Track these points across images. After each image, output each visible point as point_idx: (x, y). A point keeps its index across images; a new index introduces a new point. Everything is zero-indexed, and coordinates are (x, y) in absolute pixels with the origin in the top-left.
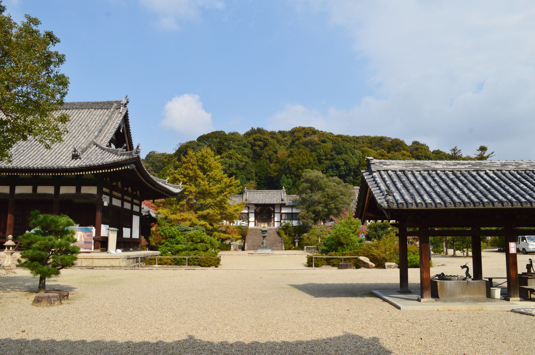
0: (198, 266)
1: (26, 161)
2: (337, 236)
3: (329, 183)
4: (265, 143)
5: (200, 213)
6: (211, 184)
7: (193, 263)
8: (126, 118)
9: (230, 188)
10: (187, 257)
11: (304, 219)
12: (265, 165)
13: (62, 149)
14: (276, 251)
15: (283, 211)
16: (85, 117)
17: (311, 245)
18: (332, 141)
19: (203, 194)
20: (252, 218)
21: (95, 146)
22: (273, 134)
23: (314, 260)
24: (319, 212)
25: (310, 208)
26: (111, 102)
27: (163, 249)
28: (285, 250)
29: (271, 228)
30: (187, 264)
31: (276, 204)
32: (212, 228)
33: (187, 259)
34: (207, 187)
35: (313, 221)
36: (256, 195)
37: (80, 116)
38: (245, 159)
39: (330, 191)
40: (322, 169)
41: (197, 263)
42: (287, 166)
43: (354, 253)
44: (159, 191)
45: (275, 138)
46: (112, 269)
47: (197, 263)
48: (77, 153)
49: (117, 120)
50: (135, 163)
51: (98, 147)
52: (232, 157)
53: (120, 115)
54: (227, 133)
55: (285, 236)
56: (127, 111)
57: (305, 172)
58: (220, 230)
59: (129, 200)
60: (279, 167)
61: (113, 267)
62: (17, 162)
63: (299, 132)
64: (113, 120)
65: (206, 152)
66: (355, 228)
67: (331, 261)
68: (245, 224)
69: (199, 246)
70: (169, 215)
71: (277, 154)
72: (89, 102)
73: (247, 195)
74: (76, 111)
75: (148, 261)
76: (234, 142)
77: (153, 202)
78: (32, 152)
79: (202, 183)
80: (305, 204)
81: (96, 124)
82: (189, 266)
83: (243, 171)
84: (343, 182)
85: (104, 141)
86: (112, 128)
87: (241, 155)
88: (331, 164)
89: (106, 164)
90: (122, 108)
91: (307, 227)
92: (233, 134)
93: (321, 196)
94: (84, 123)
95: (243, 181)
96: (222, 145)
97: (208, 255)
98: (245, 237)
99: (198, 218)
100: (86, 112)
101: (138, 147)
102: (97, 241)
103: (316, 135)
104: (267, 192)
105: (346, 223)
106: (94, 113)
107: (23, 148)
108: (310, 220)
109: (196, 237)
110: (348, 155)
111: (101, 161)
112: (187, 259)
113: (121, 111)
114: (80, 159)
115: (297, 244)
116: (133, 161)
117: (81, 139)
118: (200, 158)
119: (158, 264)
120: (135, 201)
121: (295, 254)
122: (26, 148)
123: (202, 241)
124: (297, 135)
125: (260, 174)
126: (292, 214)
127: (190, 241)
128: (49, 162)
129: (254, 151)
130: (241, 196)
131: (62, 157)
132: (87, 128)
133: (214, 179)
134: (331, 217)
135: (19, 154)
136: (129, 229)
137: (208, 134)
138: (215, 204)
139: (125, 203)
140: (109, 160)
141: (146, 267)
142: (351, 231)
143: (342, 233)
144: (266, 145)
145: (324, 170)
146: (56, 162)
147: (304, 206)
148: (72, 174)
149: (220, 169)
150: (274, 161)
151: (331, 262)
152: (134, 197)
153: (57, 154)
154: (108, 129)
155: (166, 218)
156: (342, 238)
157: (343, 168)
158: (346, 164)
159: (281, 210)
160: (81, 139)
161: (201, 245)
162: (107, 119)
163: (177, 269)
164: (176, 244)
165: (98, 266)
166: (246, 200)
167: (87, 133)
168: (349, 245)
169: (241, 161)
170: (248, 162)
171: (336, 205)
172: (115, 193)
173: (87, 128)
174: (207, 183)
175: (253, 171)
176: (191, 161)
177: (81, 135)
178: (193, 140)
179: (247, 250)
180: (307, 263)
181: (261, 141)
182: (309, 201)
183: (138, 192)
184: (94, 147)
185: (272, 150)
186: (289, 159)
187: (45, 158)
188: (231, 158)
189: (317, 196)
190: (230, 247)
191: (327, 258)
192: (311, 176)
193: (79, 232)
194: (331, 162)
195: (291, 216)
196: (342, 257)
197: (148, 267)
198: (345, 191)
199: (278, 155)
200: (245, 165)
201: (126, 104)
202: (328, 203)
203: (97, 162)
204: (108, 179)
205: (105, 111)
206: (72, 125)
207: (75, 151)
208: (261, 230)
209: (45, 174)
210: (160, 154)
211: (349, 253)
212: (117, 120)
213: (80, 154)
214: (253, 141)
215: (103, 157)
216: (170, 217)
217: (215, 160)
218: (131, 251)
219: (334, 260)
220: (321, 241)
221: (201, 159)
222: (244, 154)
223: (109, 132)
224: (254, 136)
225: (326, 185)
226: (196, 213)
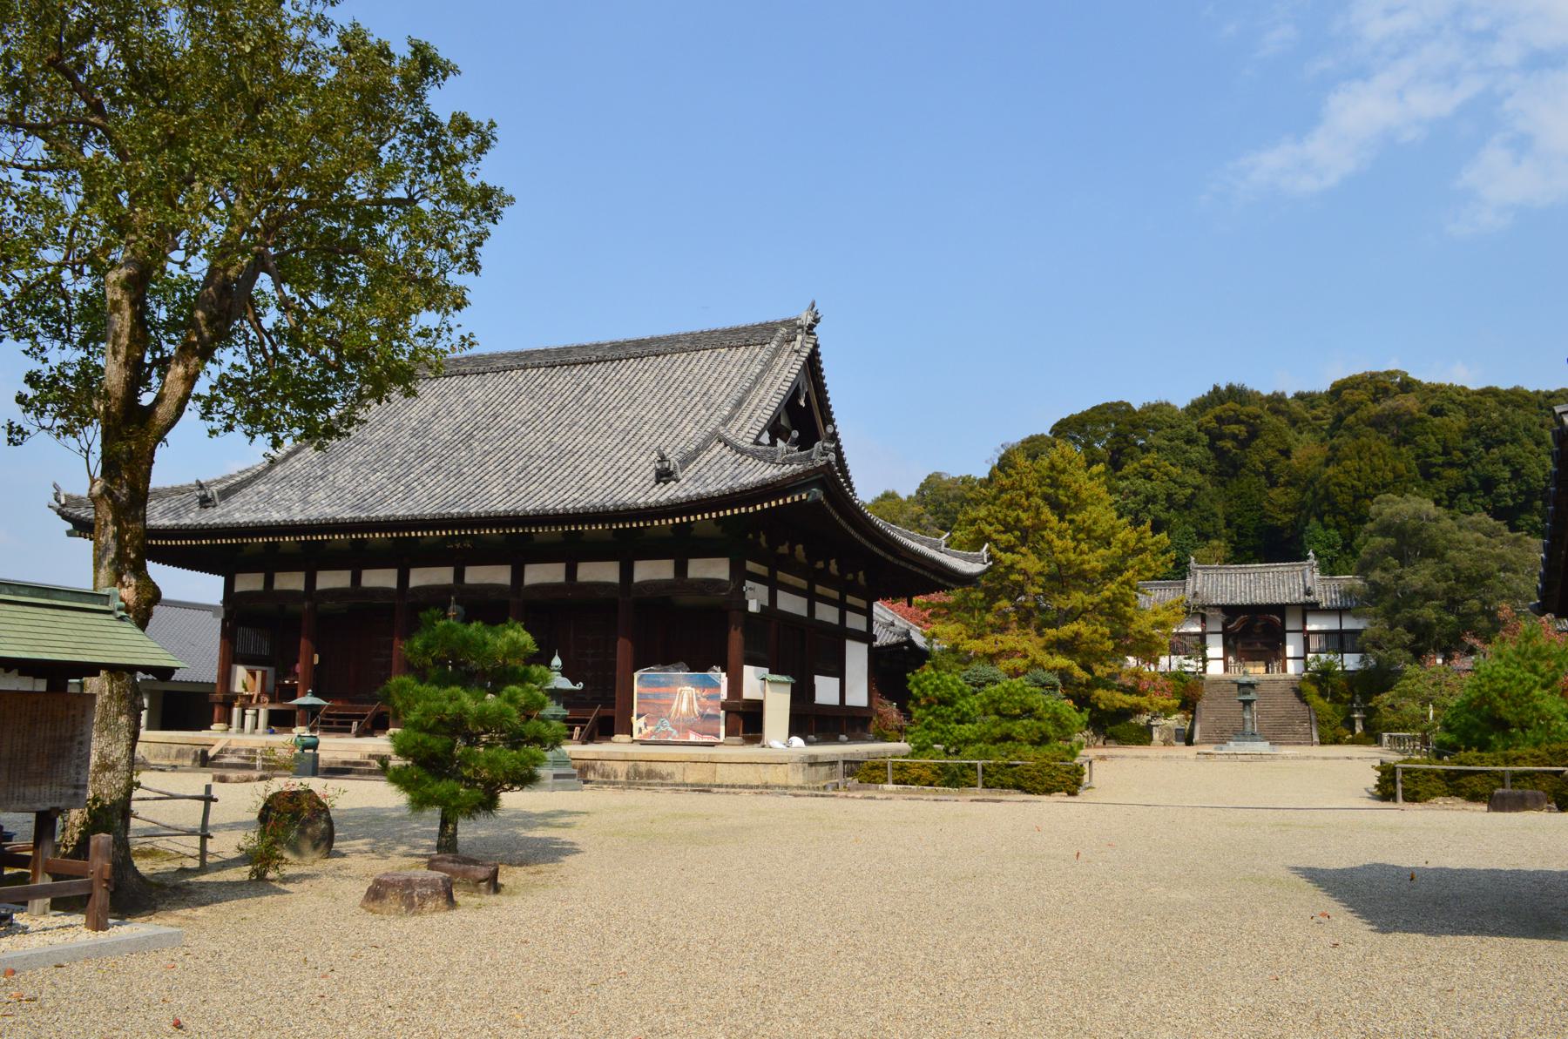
0: (1012, 791)
1: (541, 494)
2: (1483, 697)
3: (1459, 535)
4: (1251, 429)
5: (1051, 633)
6: (1084, 546)
7: (999, 779)
8: (813, 365)
9: (1140, 556)
10: (979, 763)
11: (1380, 648)
12: (1254, 492)
13: (634, 459)
14: (1284, 747)
15: (1309, 628)
16: (703, 371)
17: (1404, 728)
18: (1466, 407)
19: (1062, 579)
20: (1215, 650)
21: (722, 445)
22: (1276, 402)
23: (1399, 776)
24: (1428, 626)
25: (1399, 612)
26: (772, 324)
27: (919, 737)
28: (1322, 743)
29: (1277, 678)
30: (980, 785)
31: (1287, 604)
32: (1089, 677)
33: (979, 768)
34: (1072, 556)
35: (1409, 655)
36: (1224, 581)
37: (689, 369)
38: (1194, 478)
39: (1462, 559)
40: (1437, 496)
41: (1011, 781)
42: (1322, 492)
43: (1551, 754)
44: (910, 567)
45: (1283, 413)
46: (761, 793)
47: (1011, 781)
48: (667, 464)
49: (786, 373)
50: (821, 484)
51: (728, 448)
52: (1152, 474)
53: (794, 358)
54: (1137, 406)
55: (1321, 701)
57: (1378, 503)
58: (1119, 685)
59: (799, 586)
60: (1298, 496)
62: (519, 497)
63: (1357, 389)
64: (776, 371)
65: (1062, 456)
66: (1554, 669)
67: (1463, 781)
68: (1193, 665)
69: (1017, 728)
70: (962, 640)
71: (1289, 458)
72: (715, 331)
73: (1198, 581)
74: (682, 358)
75: (865, 773)
76: (1157, 429)
78: (560, 471)
79: (1057, 543)
80: (1381, 601)
81: (731, 386)
82: (986, 791)
83: (1186, 513)
84: (1507, 528)
85: (746, 430)
86: (771, 394)
87: (1179, 468)
88: (1466, 477)
89: (741, 492)
90: (799, 338)
91: (1390, 671)
92: (1156, 408)
93: (1433, 575)
94: (699, 386)
95: (1190, 542)
96: (1123, 440)
97: (1046, 757)
98: (1195, 706)
99: (1046, 648)
100: (706, 358)
102: (732, 712)
103: (1411, 395)
104: (1259, 570)
105: (1518, 653)
106: (728, 358)
107: (539, 461)
108: (1399, 651)
109: (1010, 702)
110: (1522, 446)
111: (730, 484)
112: (979, 768)
113: (797, 345)
114: (678, 481)
115: (1359, 729)
116: (815, 477)
117: (688, 429)
118: (1046, 473)
119: (896, 782)
120: (850, 599)
121: (1348, 758)
122: (547, 461)
123: (1029, 712)
124: (1351, 397)
125: (1239, 521)
126: (1340, 633)
127: (992, 711)
128: (596, 494)
129: (1221, 454)
130: (1179, 584)
131: (631, 479)
132: (706, 398)
133: (1089, 532)
134: (1470, 640)
135: (527, 478)
136: (836, 681)
137: (1083, 412)
138: (1096, 606)
139: (780, 593)
141: (858, 789)
142: (1537, 678)
143: (1501, 687)
144: (1253, 434)
145: (1441, 499)
147: (1379, 609)
148: (652, 523)
149: (1107, 504)
150: (1282, 479)
151: (1465, 787)
152: (846, 588)
153: (619, 473)
154: (760, 397)
155: (954, 649)
156: (1500, 702)
157: (1507, 490)
158: (1516, 474)
159: (1305, 623)
160: (688, 429)
161: (1025, 726)
162: (758, 371)
163: (946, 798)
164: (958, 722)
165: (729, 783)
166: (1195, 595)
167: (703, 411)
168: (1530, 728)
169: (1183, 485)
170: (1202, 486)
171: (1484, 603)
173: (706, 398)
174: (1072, 544)
175: (1218, 509)
176: (1025, 484)
177: (689, 418)
178: (1039, 433)
179: (1202, 743)
180: (1376, 786)
181: (1239, 422)
182: (1395, 591)
184: (718, 449)
185: (1273, 447)
186: (1331, 471)
187: (588, 485)
188: (1149, 478)
189: (1420, 576)
190: (1151, 734)
191: (1448, 772)
192: (1398, 513)
193: (686, 688)
194: (1465, 472)
195: (1339, 641)
196: (1503, 768)
197: (864, 789)
198: (1516, 556)
199: (1293, 460)
200: (1193, 494)
201: (811, 327)
202: (1458, 597)
206: (667, 395)
207: (663, 459)
208: (1234, 682)
209: (600, 527)
210: (954, 480)
211: (1532, 756)
212: (788, 370)
213: (675, 467)
214: (1214, 424)
215: (737, 471)
216: (967, 647)
217: (1091, 479)
218: (843, 743)
219: (1475, 780)
220: (1435, 717)
221: (1049, 477)
222: (1189, 464)
223: (764, 405)
224: (1218, 410)
225: (1450, 541)
226: (1041, 635)
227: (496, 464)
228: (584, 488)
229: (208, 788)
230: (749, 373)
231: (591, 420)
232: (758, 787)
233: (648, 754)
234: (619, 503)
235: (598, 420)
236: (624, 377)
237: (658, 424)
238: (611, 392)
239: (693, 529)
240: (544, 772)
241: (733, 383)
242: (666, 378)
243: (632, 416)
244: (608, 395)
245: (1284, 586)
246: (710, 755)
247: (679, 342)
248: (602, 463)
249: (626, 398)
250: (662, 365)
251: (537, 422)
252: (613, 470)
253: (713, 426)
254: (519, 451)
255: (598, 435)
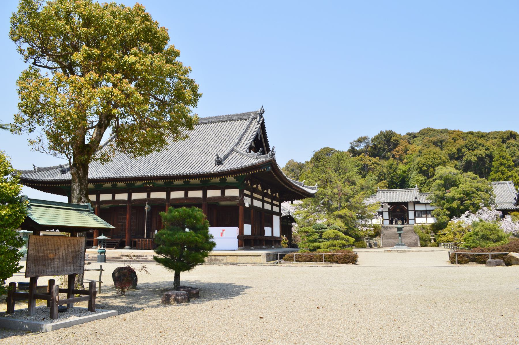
8: (262, 126)
13: (207, 157)
15: (416, 209)
21: (236, 152)
26: (249, 113)
28: (421, 246)
31: (409, 202)
33: (323, 256)
46: (254, 265)
51: (238, 153)
56: (264, 120)
61: (254, 264)
62: (170, 170)
72: (231, 115)
77: (292, 203)
101: (273, 149)
111: (241, 165)
120: (275, 202)
128: (196, 169)
131: (207, 164)
136: (271, 228)
140: (248, 164)
141: (284, 263)
146: (202, 168)
152: (273, 198)
153: (203, 162)
160: (224, 147)
162: (246, 128)
172: (255, 195)
183: (277, 194)
201: (262, 114)
203: (237, 166)
204: (249, 182)
205: (244, 121)
207: (218, 158)
212: (255, 127)
218: (252, 250)
227: (161, 159)
228: (192, 167)
229: (101, 266)
230: (242, 129)
231: (191, 144)
232: (252, 263)
233: (246, 253)
234: (204, 171)
235: (193, 144)
236: (201, 130)
237: (214, 146)
238: (197, 135)
239: (226, 180)
240: (206, 259)
241: (237, 132)
242: (215, 130)
243: (205, 143)
244: (196, 136)
245: (408, 196)
246: (235, 253)
247: (218, 118)
248: (196, 159)
249: (202, 137)
250: (213, 126)
251: (173, 145)
252: (201, 161)
253: (233, 146)
254: (168, 155)
255: (194, 149)
